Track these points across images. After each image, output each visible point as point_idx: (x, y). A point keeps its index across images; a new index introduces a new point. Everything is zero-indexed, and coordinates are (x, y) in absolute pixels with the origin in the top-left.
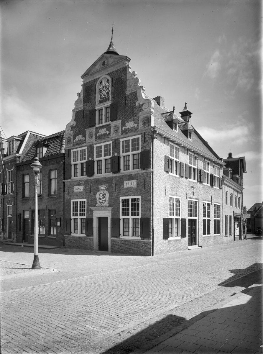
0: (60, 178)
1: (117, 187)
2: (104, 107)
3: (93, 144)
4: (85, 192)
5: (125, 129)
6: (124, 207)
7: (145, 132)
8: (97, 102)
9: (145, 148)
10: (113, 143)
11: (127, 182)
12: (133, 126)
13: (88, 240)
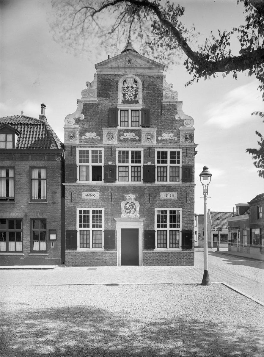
0: (55, 180)
1: (151, 197)
2: (131, 109)
3: (115, 147)
4: (102, 200)
5: (161, 139)
7: (187, 147)
8: (120, 102)
9: (187, 163)
10: (144, 151)
11: (165, 193)
12: (134, 137)
13: (107, 255)
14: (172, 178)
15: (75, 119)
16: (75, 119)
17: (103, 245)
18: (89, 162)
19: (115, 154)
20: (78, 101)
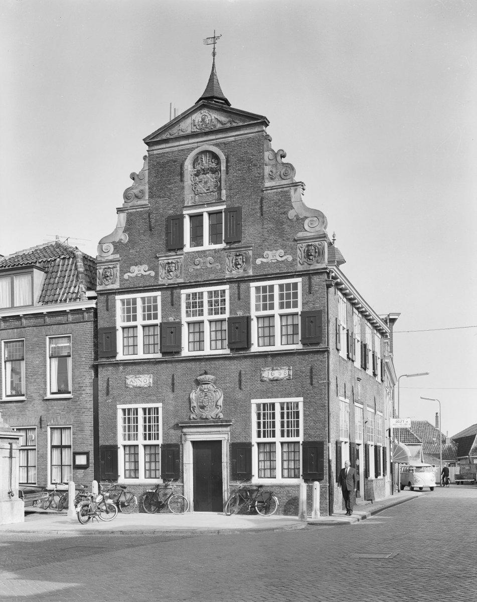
6: (297, 430)
14: (191, 345)
15: (113, 243)
16: (113, 243)
17: (301, 473)
18: (136, 321)
19: (180, 301)
20: (119, 210)
